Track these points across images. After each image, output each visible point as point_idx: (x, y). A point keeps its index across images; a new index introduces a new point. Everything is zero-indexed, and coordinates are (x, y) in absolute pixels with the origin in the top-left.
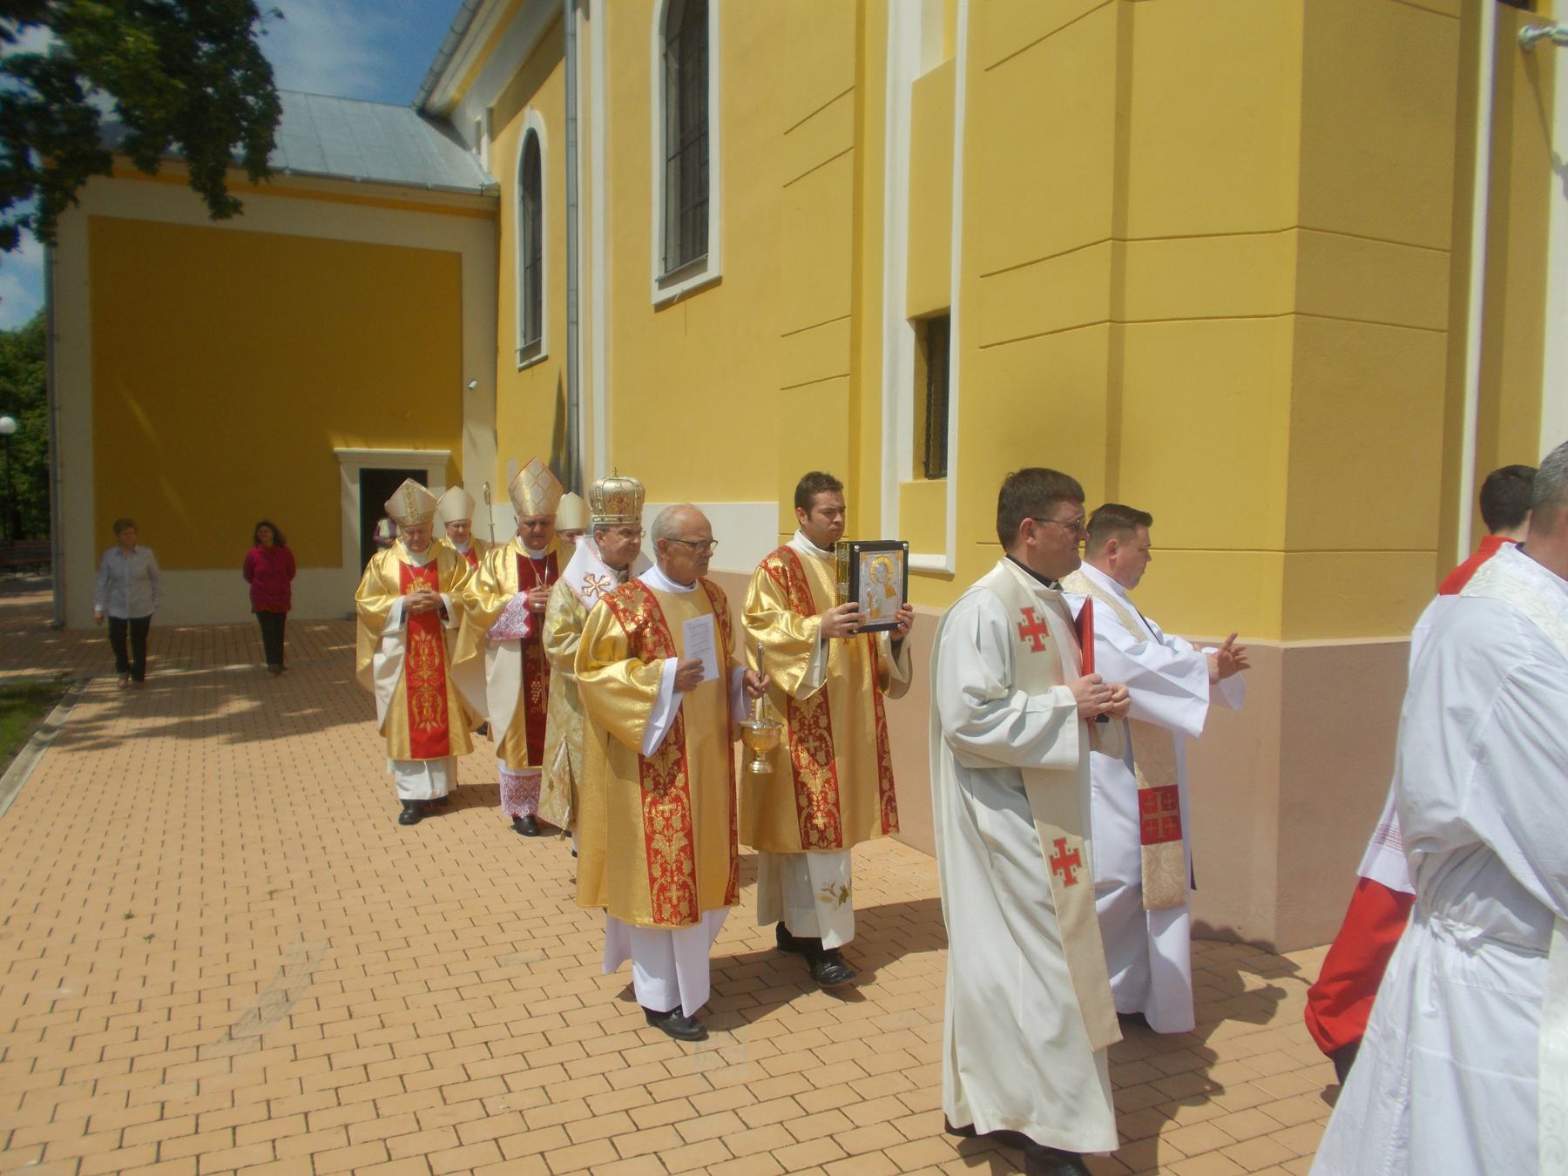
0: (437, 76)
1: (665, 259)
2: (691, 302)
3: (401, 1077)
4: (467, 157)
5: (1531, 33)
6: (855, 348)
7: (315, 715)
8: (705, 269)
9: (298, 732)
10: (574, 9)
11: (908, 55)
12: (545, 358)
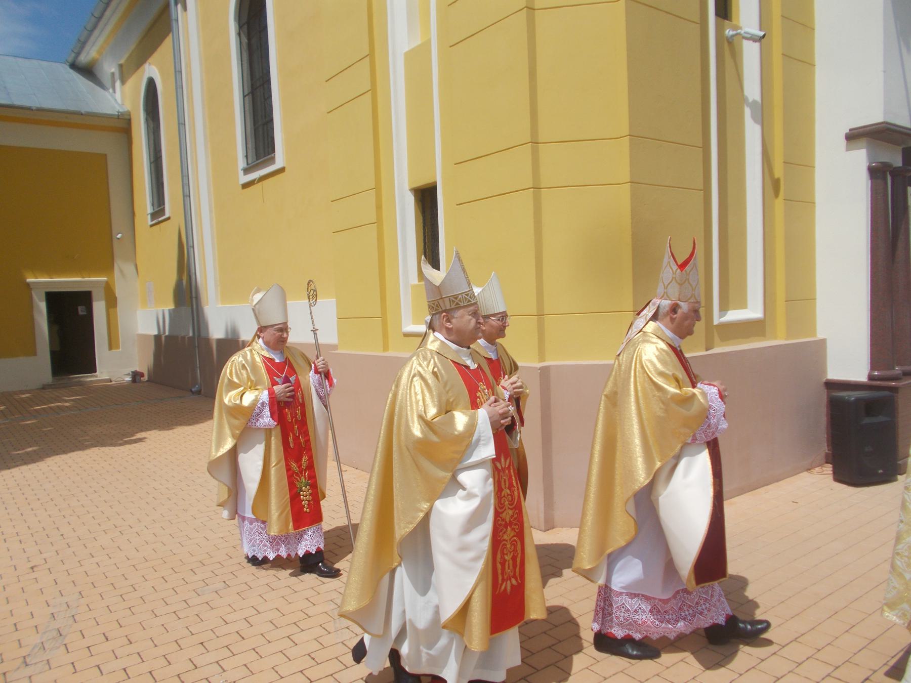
0: (83, 44)
1: (247, 156)
2: (265, 182)
3: (150, 672)
4: (107, 95)
5: (731, 33)
6: (379, 207)
7: (35, 451)
8: (274, 163)
9: (26, 463)
10: (176, 4)
11: (401, 37)
12: (169, 218)
